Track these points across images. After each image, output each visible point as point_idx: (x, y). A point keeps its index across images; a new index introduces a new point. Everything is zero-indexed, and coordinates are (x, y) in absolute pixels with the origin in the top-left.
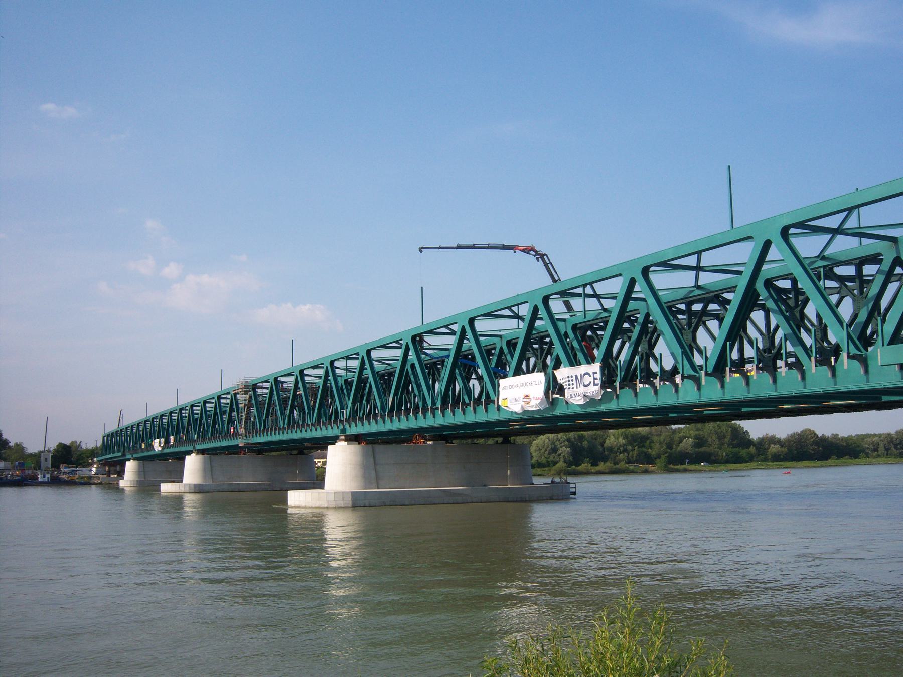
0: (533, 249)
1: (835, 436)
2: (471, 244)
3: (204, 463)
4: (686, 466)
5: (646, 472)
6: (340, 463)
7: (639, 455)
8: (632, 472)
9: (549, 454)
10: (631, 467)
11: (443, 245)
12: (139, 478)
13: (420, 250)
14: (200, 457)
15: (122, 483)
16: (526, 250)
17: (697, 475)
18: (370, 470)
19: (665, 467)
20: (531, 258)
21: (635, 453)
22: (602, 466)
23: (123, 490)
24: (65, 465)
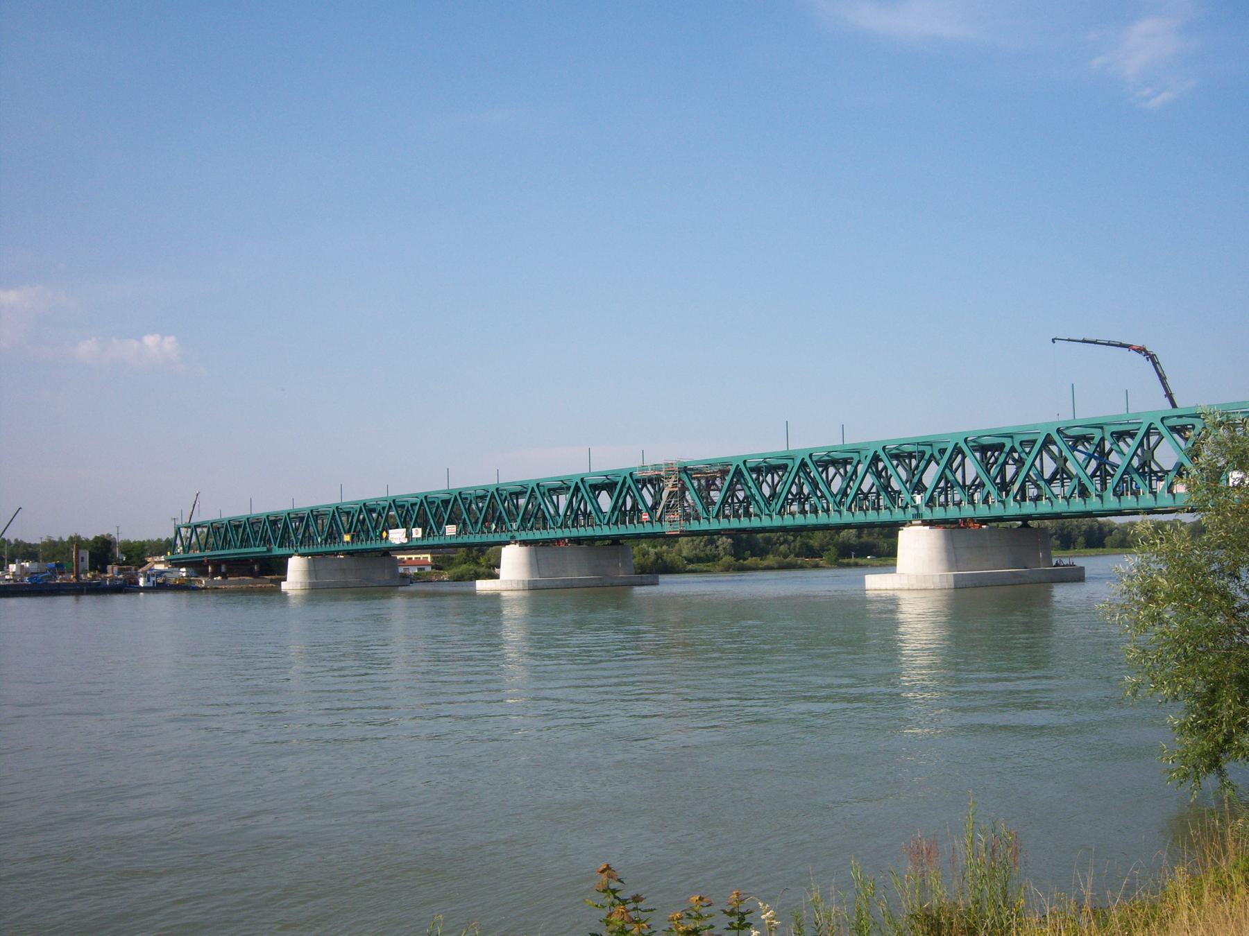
0: (1144, 350)
1: (159, 540)
2: (1094, 339)
3: (531, 556)
4: (853, 560)
5: (816, 566)
6: (513, 562)
7: (801, 547)
8: (802, 567)
9: (706, 545)
10: (799, 561)
11: (1087, 338)
12: (532, 573)
13: (1053, 341)
14: (524, 549)
15: (284, 586)
16: (1141, 350)
17: (799, 573)
18: (535, 564)
19: (836, 560)
20: (1141, 358)
21: (798, 544)
22: (771, 560)
23: (286, 593)
24: (97, 568)
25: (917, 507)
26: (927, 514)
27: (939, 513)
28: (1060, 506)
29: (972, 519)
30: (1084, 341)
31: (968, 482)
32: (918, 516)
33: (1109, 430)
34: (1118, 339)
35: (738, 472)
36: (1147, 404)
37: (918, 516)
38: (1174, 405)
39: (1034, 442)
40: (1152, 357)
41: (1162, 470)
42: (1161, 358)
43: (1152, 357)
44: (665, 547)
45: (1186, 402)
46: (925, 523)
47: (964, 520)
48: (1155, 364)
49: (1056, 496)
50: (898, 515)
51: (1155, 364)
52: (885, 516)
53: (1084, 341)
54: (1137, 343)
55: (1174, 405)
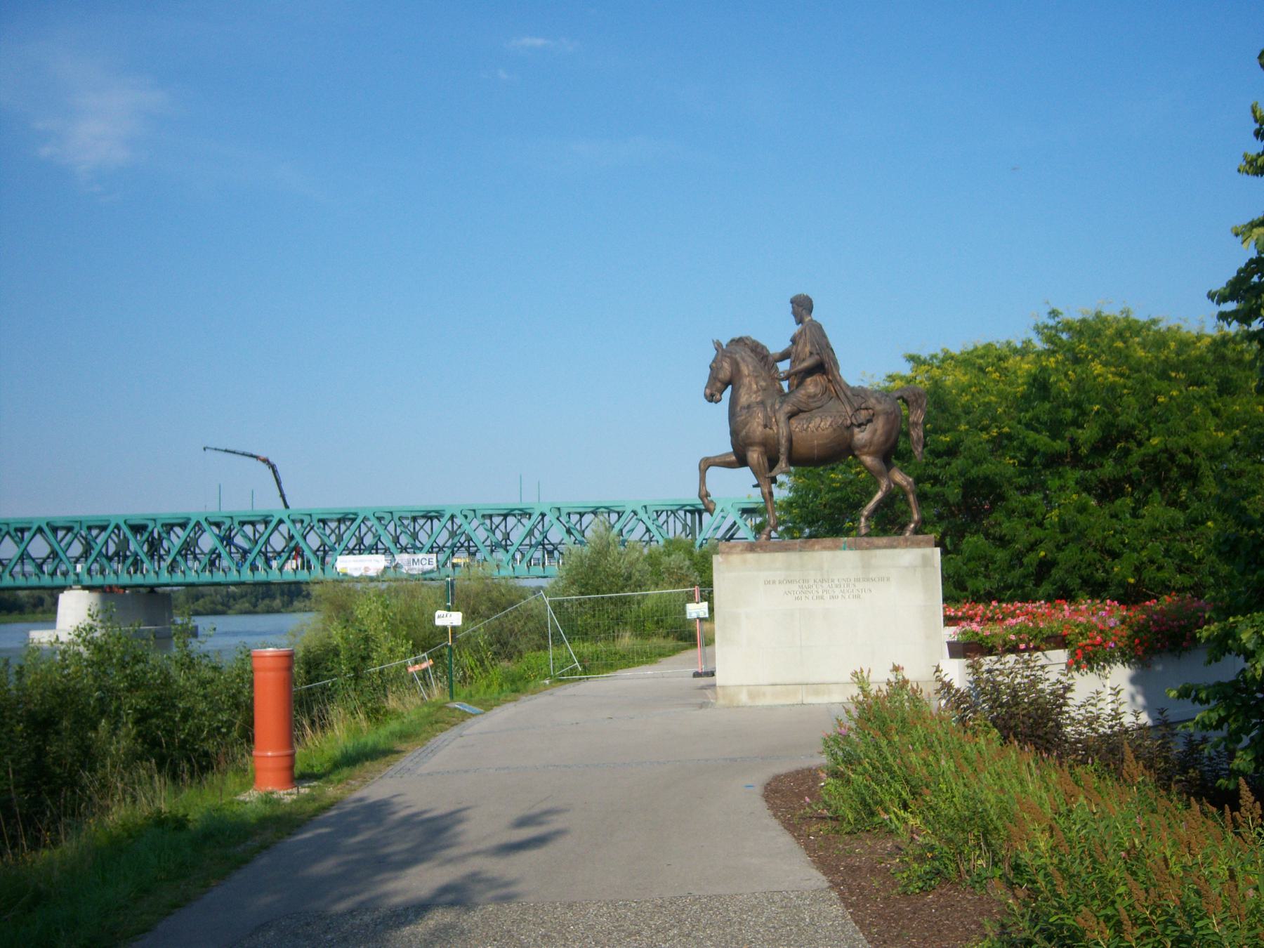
16: (266, 461)
20: (265, 467)
25: (77, 575)
26: (87, 580)
27: (98, 580)
28: (192, 577)
29: (117, 586)
30: (226, 451)
31: (110, 553)
32: (78, 582)
33: (315, 518)
34: (248, 451)
35: (198, 524)
36: (271, 505)
37: (78, 582)
38: (287, 506)
39: (29, 529)
40: (273, 467)
41: (275, 551)
42: (279, 468)
43: (273, 467)
44: (1093, 503)
45: (299, 504)
46: (85, 588)
47: (110, 587)
48: (275, 472)
49: (190, 569)
50: (59, 580)
51: (275, 472)
52: (46, 580)
53: (226, 451)
54: (263, 455)
55: (287, 506)
